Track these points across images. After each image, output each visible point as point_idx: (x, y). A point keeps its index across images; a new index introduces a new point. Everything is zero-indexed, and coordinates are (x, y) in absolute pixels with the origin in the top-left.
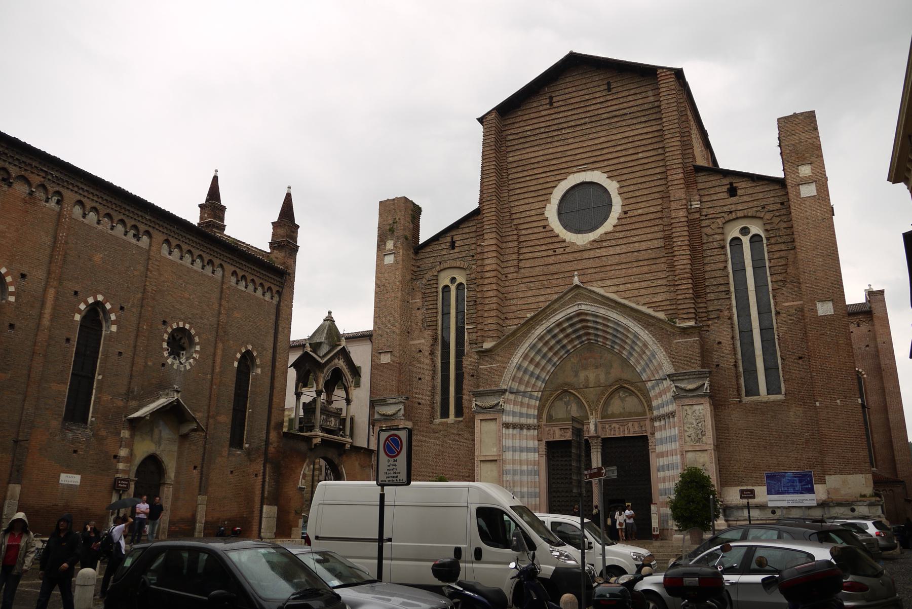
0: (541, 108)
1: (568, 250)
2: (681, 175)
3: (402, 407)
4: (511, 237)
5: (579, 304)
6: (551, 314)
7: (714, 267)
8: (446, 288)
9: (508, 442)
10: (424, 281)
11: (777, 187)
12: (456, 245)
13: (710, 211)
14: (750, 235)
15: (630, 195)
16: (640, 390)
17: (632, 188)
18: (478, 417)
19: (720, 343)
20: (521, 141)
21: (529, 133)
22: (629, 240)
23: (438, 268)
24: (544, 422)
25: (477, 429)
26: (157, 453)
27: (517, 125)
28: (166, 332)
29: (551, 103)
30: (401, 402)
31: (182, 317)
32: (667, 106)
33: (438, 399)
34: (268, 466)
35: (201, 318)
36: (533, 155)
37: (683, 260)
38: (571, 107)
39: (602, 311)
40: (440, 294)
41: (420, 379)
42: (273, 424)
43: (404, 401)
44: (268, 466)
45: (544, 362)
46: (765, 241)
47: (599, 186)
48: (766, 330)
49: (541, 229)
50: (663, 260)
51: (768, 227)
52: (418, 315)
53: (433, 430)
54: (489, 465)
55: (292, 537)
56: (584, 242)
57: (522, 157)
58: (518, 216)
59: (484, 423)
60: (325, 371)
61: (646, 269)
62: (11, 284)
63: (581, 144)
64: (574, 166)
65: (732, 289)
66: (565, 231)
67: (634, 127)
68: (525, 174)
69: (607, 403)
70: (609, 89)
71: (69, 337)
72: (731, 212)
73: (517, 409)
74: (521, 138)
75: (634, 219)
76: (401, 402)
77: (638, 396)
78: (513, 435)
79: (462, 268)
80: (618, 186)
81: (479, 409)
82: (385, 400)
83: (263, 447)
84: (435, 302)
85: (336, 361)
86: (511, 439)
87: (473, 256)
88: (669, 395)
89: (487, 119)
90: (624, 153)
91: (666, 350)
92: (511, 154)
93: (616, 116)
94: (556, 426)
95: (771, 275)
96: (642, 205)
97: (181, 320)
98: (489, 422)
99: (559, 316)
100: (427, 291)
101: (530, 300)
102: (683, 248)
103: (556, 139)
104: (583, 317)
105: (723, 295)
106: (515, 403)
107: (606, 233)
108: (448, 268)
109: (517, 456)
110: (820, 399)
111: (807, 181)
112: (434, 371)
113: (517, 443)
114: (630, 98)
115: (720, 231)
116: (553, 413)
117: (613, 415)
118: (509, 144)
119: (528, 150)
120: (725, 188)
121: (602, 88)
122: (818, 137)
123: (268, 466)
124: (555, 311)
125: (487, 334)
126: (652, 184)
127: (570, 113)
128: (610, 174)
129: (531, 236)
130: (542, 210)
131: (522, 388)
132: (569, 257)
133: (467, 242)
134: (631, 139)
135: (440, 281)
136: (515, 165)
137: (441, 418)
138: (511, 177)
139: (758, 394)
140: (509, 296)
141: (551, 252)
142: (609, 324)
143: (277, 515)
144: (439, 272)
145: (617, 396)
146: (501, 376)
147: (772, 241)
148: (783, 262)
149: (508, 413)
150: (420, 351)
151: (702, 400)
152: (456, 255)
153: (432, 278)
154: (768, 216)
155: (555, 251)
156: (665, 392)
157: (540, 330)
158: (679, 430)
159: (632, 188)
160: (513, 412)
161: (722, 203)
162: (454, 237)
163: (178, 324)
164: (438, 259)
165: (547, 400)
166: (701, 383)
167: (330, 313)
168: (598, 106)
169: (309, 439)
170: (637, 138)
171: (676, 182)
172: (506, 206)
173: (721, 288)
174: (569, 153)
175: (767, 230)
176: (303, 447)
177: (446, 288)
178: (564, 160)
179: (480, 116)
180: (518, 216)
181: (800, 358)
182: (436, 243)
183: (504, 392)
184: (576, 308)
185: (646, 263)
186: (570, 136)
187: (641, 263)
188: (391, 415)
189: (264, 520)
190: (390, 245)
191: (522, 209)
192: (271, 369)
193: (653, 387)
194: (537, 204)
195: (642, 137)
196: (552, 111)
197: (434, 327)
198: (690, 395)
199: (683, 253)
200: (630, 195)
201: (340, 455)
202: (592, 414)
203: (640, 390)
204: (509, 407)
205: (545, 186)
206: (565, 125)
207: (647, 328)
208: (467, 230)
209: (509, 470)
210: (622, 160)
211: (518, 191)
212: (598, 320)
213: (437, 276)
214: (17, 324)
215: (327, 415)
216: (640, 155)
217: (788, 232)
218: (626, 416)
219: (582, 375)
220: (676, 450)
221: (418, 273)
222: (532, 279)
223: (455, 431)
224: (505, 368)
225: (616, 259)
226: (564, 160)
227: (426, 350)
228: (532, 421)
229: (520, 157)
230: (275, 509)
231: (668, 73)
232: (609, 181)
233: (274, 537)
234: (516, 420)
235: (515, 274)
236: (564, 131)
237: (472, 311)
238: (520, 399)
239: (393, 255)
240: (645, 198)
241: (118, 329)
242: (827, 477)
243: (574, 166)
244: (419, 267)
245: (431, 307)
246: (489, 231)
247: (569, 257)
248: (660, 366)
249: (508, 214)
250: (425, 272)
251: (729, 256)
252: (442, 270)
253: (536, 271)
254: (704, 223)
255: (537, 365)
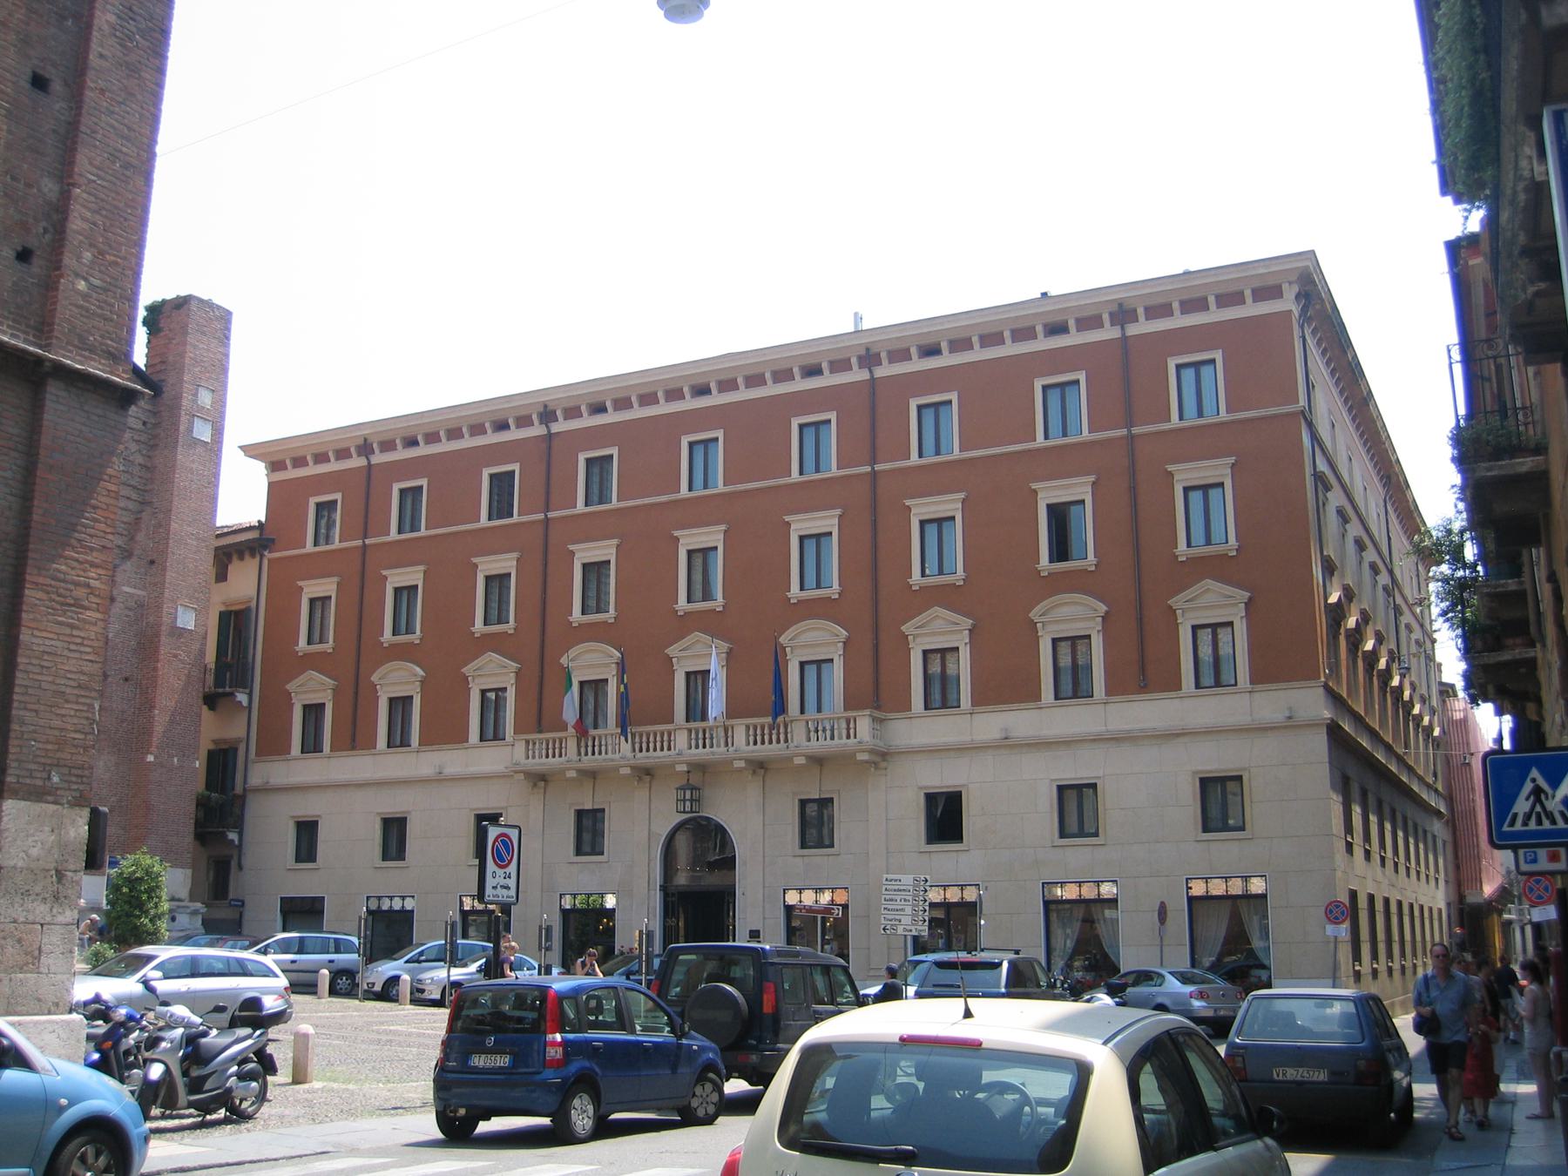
122: (227, 355)
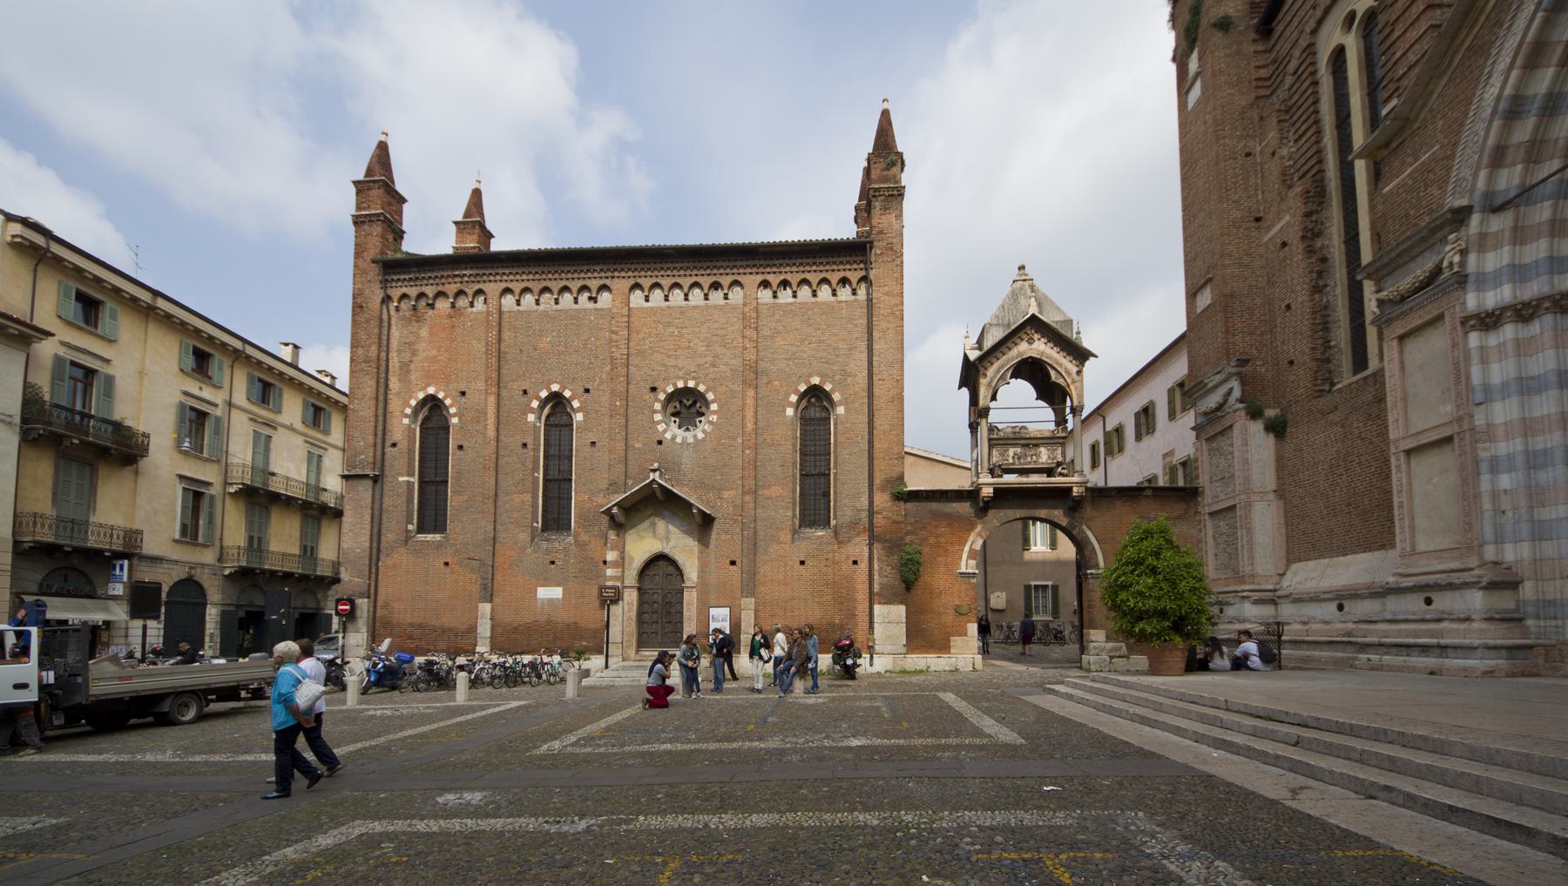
26: (665, 551)
28: (657, 400)
31: (681, 374)
34: (877, 547)
35: (714, 365)
42: (877, 482)
43: (1234, 370)
55: (952, 651)
62: (452, 406)
71: (524, 441)
83: (865, 520)
97: (679, 378)
143: (907, 618)
149: (1483, 281)
163: (675, 385)
192: (866, 401)
214: (465, 444)
230: (901, 610)
241: (584, 416)
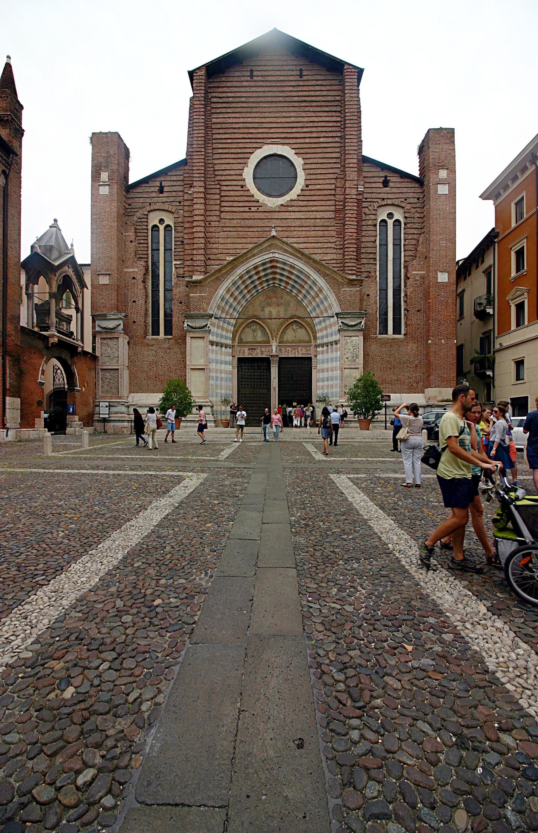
0: (243, 79)
1: (260, 209)
2: (355, 161)
3: (121, 322)
4: (214, 190)
5: (273, 253)
6: (251, 257)
7: (367, 239)
8: (155, 228)
9: (212, 356)
10: (135, 219)
11: (417, 186)
12: (165, 190)
13: (369, 196)
14: (394, 219)
15: (312, 172)
16: (308, 324)
17: (313, 166)
18: (188, 336)
19: (368, 295)
20: (225, 105)
21: (231, 99)
22: (309, 209)
23: (148, 208)
24: (236, 344)
25: (188, 345)
27: (221, 90)
29: (252, 76)
30: (121, 319)
32: (350, 99)
33: (150, 320)
36: (234, 120)
37: (351, 230)
38: (269, 84)
39: (291, 260)
40: (150, 231)
41: (134, 302)
44: (8, 358)
45: (240, 297)
46: (403, 225)
47: (284, 160)
48: (397, 292)
49: (239, 188)
50: (334, 228)
51: (407, 215)
52: (131, 248)
53: (147, 344)
54: (197, 372)
56: (274, 204)
57: (225, 121)
58: (220, 173)
59: (193, 340)
60: (57, 274)
61: (320, 233)
63: (274, 120)
64: (269, 138)
65: (378, 258)
66: (259, 193)
67: (319, 114)
68: (227, 136)
69: (283, 332)
70: (301, 76)
72: (383, 199)
73: (220, 331)
74: (224, 103)
75: (313, 193)
76: (121, 319)
77: (306, 329)
78: (216, 351)
79: (170, 212)
80: (303, 162)
81: (190, 329)
82: (105, 315)
84: (146, 238)
85: (66, 268)
86: (216, 353)
87: (180, 202)
88: (336, 328)
89: (198, 74)
90: (309, 135)
91: (336, 295)
92: (215, 116)
93: (305, 101)
94: (245, 346)
95: (405, 251)
96: (321, 182)
98: (198, 339)
99: (257, 260)
100: (138, 227)
101: (229, 246)
102: (352, 219)
103: (254, 110)
104: (275, 264)
105: (372, 261)
106: (218, 327)
107: (291, 200)
108: (158, 210)
109: (219, 367)
110: (432, 338)
111: (442, 182)
112: (147, 296)
113: (219, 357)
114: (317, 88)
115: (374, 212)
116: (243, 337)
117: (287, 342)
118: (214, 105)
119: (230, 115)
120: (381, 180)
121: (295, 73)
122: (454, 149)
123: (7, 358)
124: (254, 255)
125: (195, 268)
126: (329, 166)
127: (267, 89)
128: (297, 151)
129: (231, 192)
130: (240, 171)
131: (224, 316)
132: (262, 215)
133: (175, 189)
134: (316, 124)
135: (149, 221)
136: (219, 126)
137: (152, 335)
138: (215, 136)
139: (387, 333)
140: (212, 240)
141: (247, 209)
142: (294, 272)
144: (149, 212)
145: (291, 327)
146: (208, 304)
147: (408, 226)
148: (414, 242)
150: (134, 278)
151: (357, 333)
152: (165, 200)
153: (143, 216)
154: (408, 207)
155: (250, 209)
156: (331, 326)
157: (240, 270)
158: (341, 354)
159: (313, 166)
160: (217, 334)
161: (379, 191)
162: (163, 183)
164: (148, 200)
165: (240, 327)
166: (359, 321)
167: (55, 221)
168: (291, 89)
169: (46, 338)
170: (320, 124)
171: (351, 165)
172: (211, 162)
173: (371, 256)
174: (265, 125)
175: (406, 217)
176: (40, 344)
177: (155, 228)
178: (260, 131)
179: (191, 69)
180: (220, 173)
181: (419, 311)
182: (147, 185)
183: (211, 316)
184: (271, 255)
185: (321, 228)
186: (266, 110)
187: (317, 228)
188: (112, 329)
189: (7, 411)
190: (104, 176)
191: (223, 167)
193: (320, 323)
194: (236, 165)
195: (323, 124)
196: (252, 84)
197: (146, 260)
198: (351, 329)
199: (352, 223)
200: (312, 172)
201: (72, 357)
202: (273, 339)
203: (308, 324)
204: (213, 329)
205: (244, 151)
206: (263, 100)
207: (324, 277)
208: (175, 178)
209: (213, 377)
210: (307, 140)
211: (220, 151)
212: (286, 268)
213: (147, 215)
215: (60, 319)
216: (322, 140)
217: (420, 220)
218: (296, 344)
219: (267, 310)
220: (336, 367)
221: (129, 210)
222: (232, 229)
223: (166, 345)
224: (212, 298)
225: (298, 223)
226: (260, 131)
227: (140, 277)
228: (229, 342)
229: (223, 120)
231: (353, 70)
232: (295, 156)
233: (19, 427)
234: (218, 340)
235: (217, 223)
236: (261, 105)
237: (179, 250)
238: (221, 324)
239: (108, 187)
240: (322, 177)
242: (426, 390)
243: (269, 138)
244: (130, 205)
245: (142, 241)
246: (198, 179)
247: (262, 215)
248: (330, 306)
249: (212, 169)
250: (136, 210)
251: (378, 233)
252: (151, 211)
253: (234, 223)
254: (364, 205)
255: (235, 299)
